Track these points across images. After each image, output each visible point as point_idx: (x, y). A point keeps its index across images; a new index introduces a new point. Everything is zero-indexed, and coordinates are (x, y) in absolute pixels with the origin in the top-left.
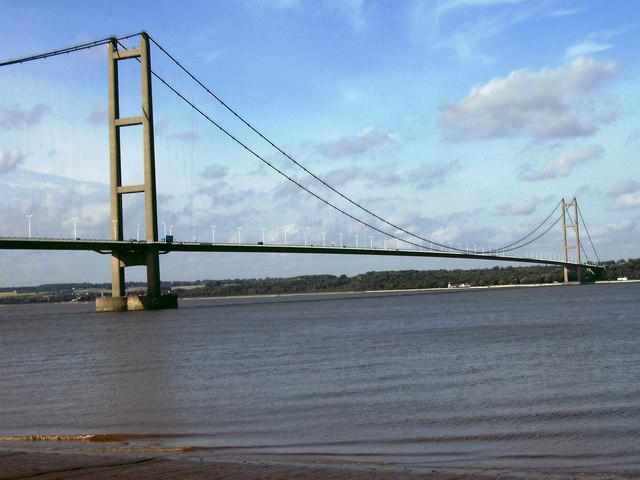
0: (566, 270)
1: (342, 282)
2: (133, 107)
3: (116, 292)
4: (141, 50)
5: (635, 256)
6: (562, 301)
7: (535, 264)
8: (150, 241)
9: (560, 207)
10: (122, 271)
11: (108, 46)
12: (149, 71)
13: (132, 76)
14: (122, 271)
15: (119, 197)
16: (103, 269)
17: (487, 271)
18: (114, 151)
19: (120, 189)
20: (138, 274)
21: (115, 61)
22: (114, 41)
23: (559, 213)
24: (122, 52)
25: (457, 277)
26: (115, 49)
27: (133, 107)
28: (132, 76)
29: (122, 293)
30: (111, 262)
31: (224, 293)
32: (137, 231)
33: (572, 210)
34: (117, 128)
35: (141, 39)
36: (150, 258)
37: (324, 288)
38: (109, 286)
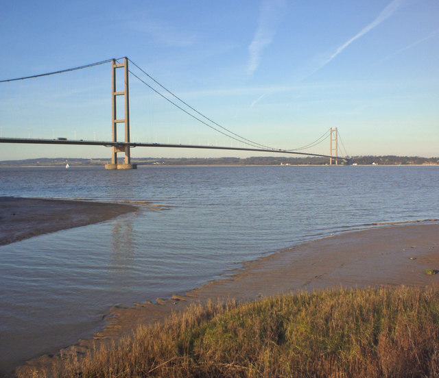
1: (236, 161)
2: (121, 88)
3: (113, 162)
4: (124, 64)
5: (3, 247)
6: (336, 315)
7: (307, 156)
8: (127, 142)
10: (116, 154)
11: (112, 62)
12: (127, 71)
13: (121, 73)
14: (116, 154)
15: (115, 124)
16: (108, 152)
17: (294, 158)
18: (113, 106)
19: (115, 121)
20: (121, 154)
21: (115, 68)
22: (114, 60)
24: (118, 64)
25: (284, 160)
26: (115, 64)
27: (121, 88)
28: (121, 73)
29: (116, 162)
30: (111, 150)
31: (174, 164)
32: (121, 138)
33: (335, 132)
34: (115, 96)
35: (124, 60)
36: (126, 148)
37: (203, 164)
38: (111, 159)
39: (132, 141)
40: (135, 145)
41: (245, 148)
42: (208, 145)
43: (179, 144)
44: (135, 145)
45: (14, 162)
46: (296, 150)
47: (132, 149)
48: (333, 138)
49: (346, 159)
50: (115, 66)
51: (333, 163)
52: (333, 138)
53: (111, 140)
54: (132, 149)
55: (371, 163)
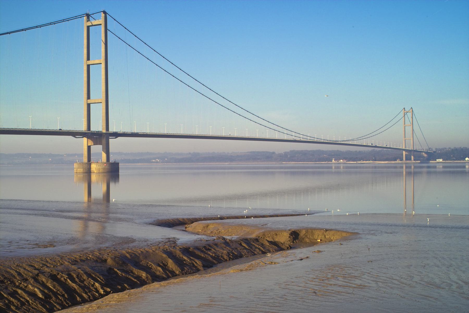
0: (404, 152)
8: (104, 131)
9: (402, 113)
11: (85, 18)
15: (89, 105)
19: (89, 101)
20: (97, 149)
23: (402, 114)
33: (409, 115)
36: (104, 141)
37: (258, 169)
39: (112, 129)
40: (116, 135)
41: (268, 137)
42: (224, 135)
43: (56, 127)
44: (116, 135)
45: (105, 119)
46: (353, 140)
47: (112, 141)
48: (408, 123)
49: (426, 153)
50: (89, 24)
51: (408, 158)
52: (408, 123)
53: (83, 128)
54: (112, 141)
55: (464, 159)
